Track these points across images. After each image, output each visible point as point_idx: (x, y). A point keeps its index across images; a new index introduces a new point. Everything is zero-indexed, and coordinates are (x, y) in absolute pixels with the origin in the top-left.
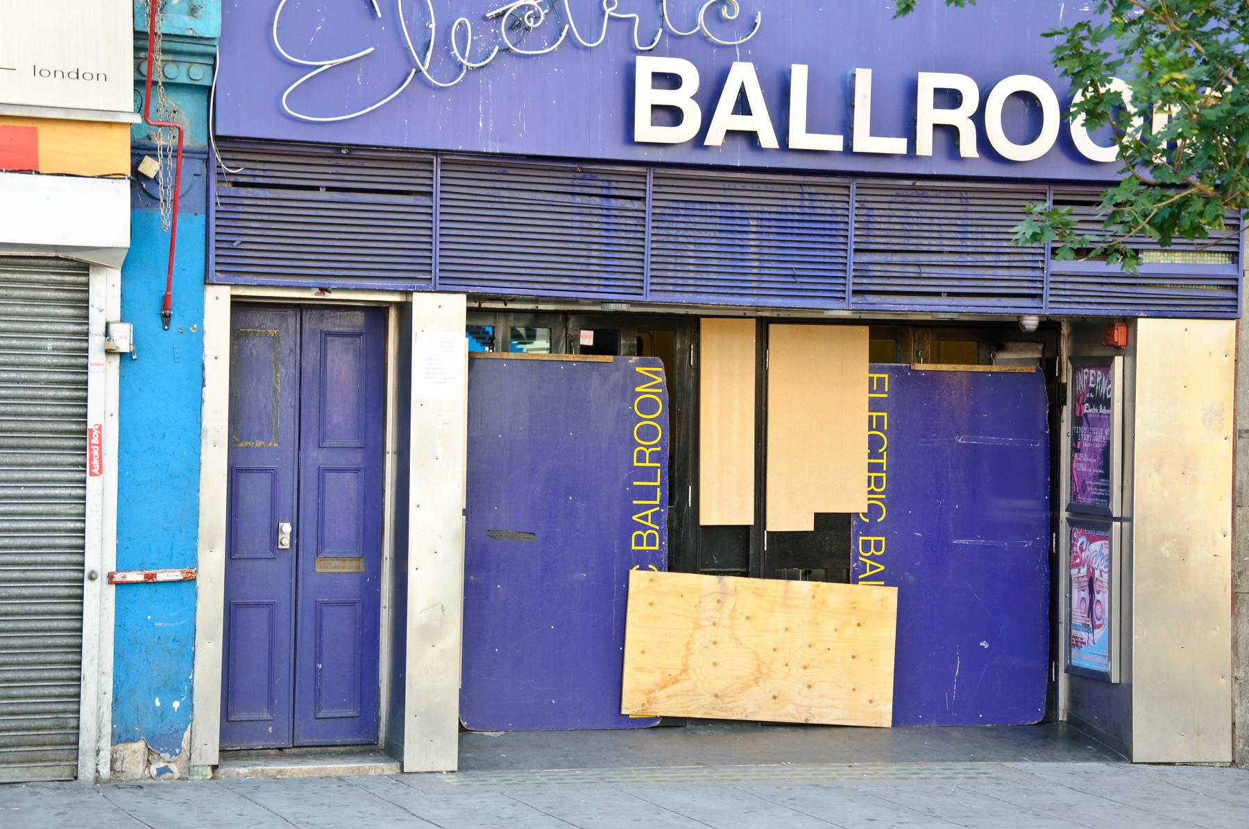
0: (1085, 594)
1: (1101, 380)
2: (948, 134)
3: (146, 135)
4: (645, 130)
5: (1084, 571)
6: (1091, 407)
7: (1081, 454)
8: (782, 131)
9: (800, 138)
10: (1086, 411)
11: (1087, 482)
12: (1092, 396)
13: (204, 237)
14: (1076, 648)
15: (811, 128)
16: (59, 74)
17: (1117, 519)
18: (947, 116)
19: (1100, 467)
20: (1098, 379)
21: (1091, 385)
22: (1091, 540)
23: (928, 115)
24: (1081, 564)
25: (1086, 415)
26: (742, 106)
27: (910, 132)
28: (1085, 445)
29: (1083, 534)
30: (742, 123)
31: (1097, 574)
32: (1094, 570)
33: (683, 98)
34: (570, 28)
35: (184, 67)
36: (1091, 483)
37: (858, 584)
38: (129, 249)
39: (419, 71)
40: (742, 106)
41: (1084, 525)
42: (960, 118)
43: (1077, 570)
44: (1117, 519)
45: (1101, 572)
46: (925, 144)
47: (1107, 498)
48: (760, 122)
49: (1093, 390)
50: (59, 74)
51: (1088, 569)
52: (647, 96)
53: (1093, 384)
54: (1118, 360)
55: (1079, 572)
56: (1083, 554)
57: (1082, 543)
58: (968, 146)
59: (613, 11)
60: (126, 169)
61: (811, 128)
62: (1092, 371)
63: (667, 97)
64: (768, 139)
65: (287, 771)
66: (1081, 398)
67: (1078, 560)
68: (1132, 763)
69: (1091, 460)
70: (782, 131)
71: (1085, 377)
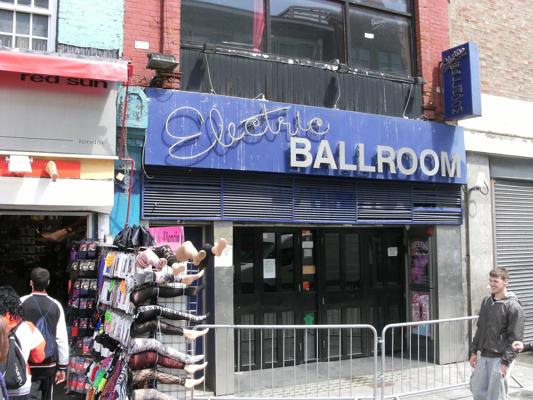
0: (418, 312)
1: (423, 245)
2: (386, 166)
3: (119, 165)
4: (294, 163)
5: (417, 304)
6: (419, 253)
7: (415, 268)
8: (338, 164)
9: (344, 166)
10: (416, 254)
11: (418, 277)
12: (419, 250)
13: (139, 200)
14: (415, 328)
15: (347, 162)
16: (89, 142)
17: (431, 288)
18: (386, 160)
19: (424, 272)
20: (421, 244)
21: (418, 246)
22: (420, 295)
23: (381, 161)
24: (416, 302)
25: (416, 256)
26: (324, 155)
27: (376, 165)
28: (416, 265)
29: (416, 293)
30: (325, 161)
31: (423, 305)
32: (422, 304)
33: (306, 152)
34: (268, 127)
35: (133, 141)
36: (419, 277)
37: (8, 162)
38: (113, 206)
39: (217, 141)
40: (324, 155)
41: (413, 290)
42: (390, 161)
43: (414, 304)
44: (431, 288)
45: (425, 305)
46: (381, 170)
47: (428, 282)
48: (330, 160)
49: (419, 248)
50: (89, 142)
51: (419, 304)
52: (294, 152)
53: (419, 246)
54: (430, 238)
55: (416, 305)
56: (417, 299)
57: (416, 296)
58: (393, 171)
59: (283, 122)
60: (113, 178)
61: (347, 162)
62: (418, 242)
63: (300, 151)
64: (333, 166)
65: (164, 240)
66: (414, 250)
67: (415, 301)
68: (439, 365)
69: (419, 270)
70: (338, 164)
71: (416, 244)
